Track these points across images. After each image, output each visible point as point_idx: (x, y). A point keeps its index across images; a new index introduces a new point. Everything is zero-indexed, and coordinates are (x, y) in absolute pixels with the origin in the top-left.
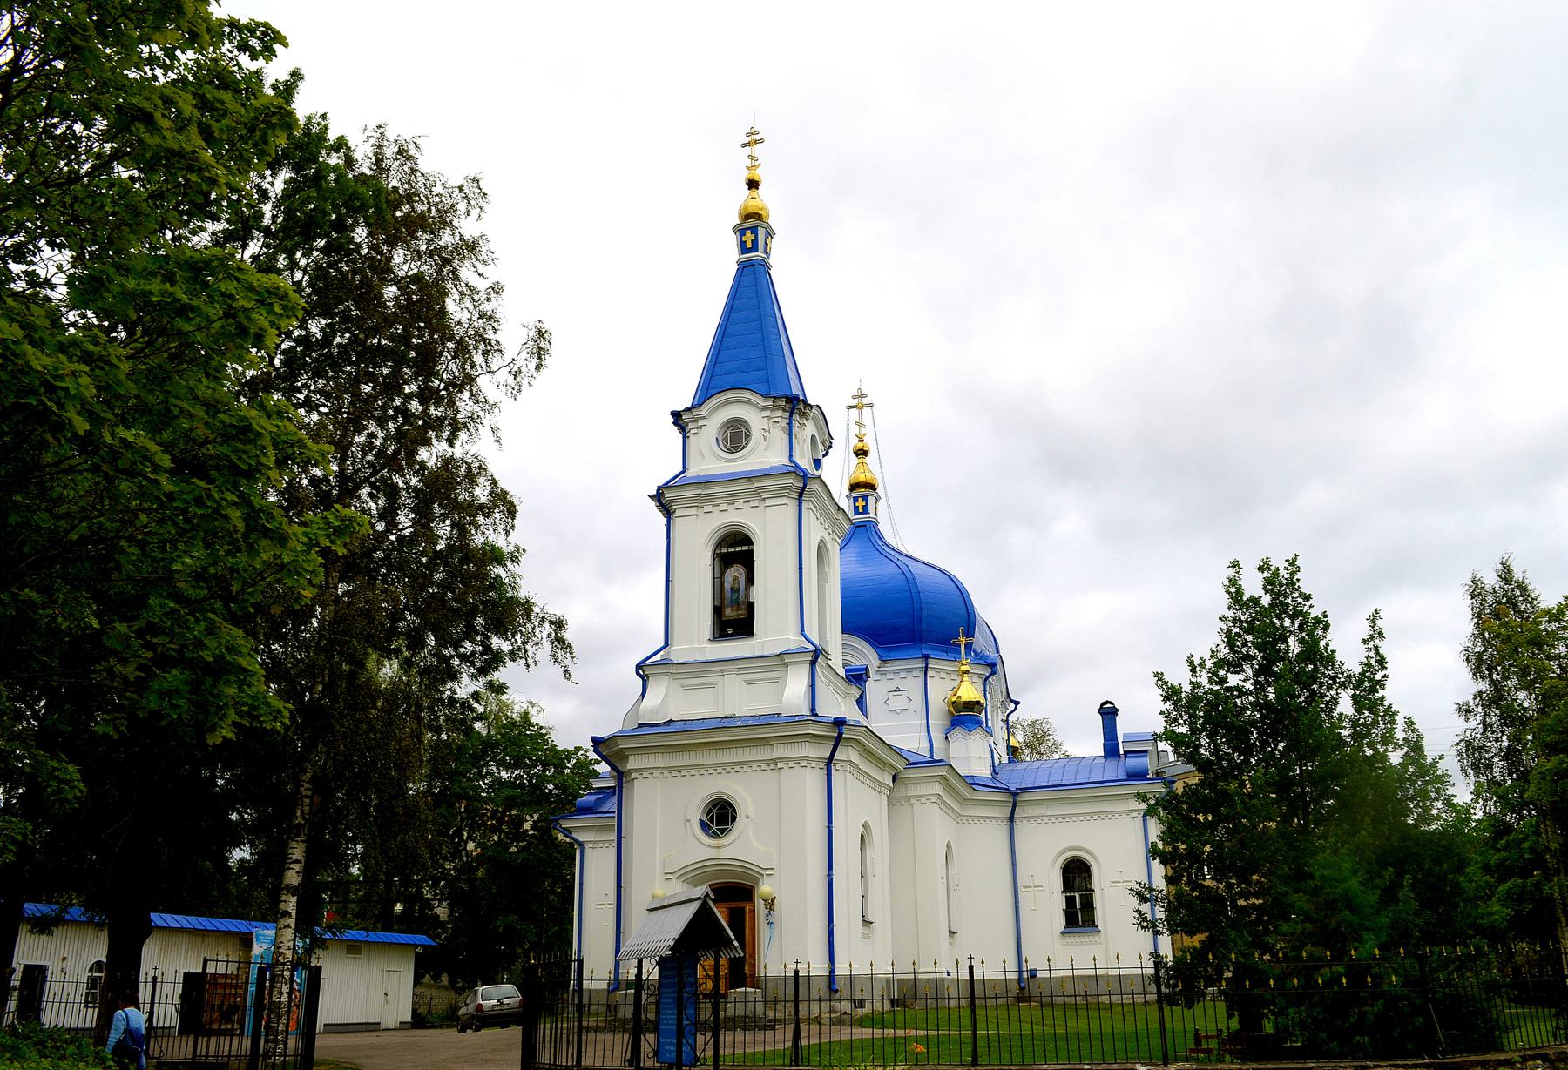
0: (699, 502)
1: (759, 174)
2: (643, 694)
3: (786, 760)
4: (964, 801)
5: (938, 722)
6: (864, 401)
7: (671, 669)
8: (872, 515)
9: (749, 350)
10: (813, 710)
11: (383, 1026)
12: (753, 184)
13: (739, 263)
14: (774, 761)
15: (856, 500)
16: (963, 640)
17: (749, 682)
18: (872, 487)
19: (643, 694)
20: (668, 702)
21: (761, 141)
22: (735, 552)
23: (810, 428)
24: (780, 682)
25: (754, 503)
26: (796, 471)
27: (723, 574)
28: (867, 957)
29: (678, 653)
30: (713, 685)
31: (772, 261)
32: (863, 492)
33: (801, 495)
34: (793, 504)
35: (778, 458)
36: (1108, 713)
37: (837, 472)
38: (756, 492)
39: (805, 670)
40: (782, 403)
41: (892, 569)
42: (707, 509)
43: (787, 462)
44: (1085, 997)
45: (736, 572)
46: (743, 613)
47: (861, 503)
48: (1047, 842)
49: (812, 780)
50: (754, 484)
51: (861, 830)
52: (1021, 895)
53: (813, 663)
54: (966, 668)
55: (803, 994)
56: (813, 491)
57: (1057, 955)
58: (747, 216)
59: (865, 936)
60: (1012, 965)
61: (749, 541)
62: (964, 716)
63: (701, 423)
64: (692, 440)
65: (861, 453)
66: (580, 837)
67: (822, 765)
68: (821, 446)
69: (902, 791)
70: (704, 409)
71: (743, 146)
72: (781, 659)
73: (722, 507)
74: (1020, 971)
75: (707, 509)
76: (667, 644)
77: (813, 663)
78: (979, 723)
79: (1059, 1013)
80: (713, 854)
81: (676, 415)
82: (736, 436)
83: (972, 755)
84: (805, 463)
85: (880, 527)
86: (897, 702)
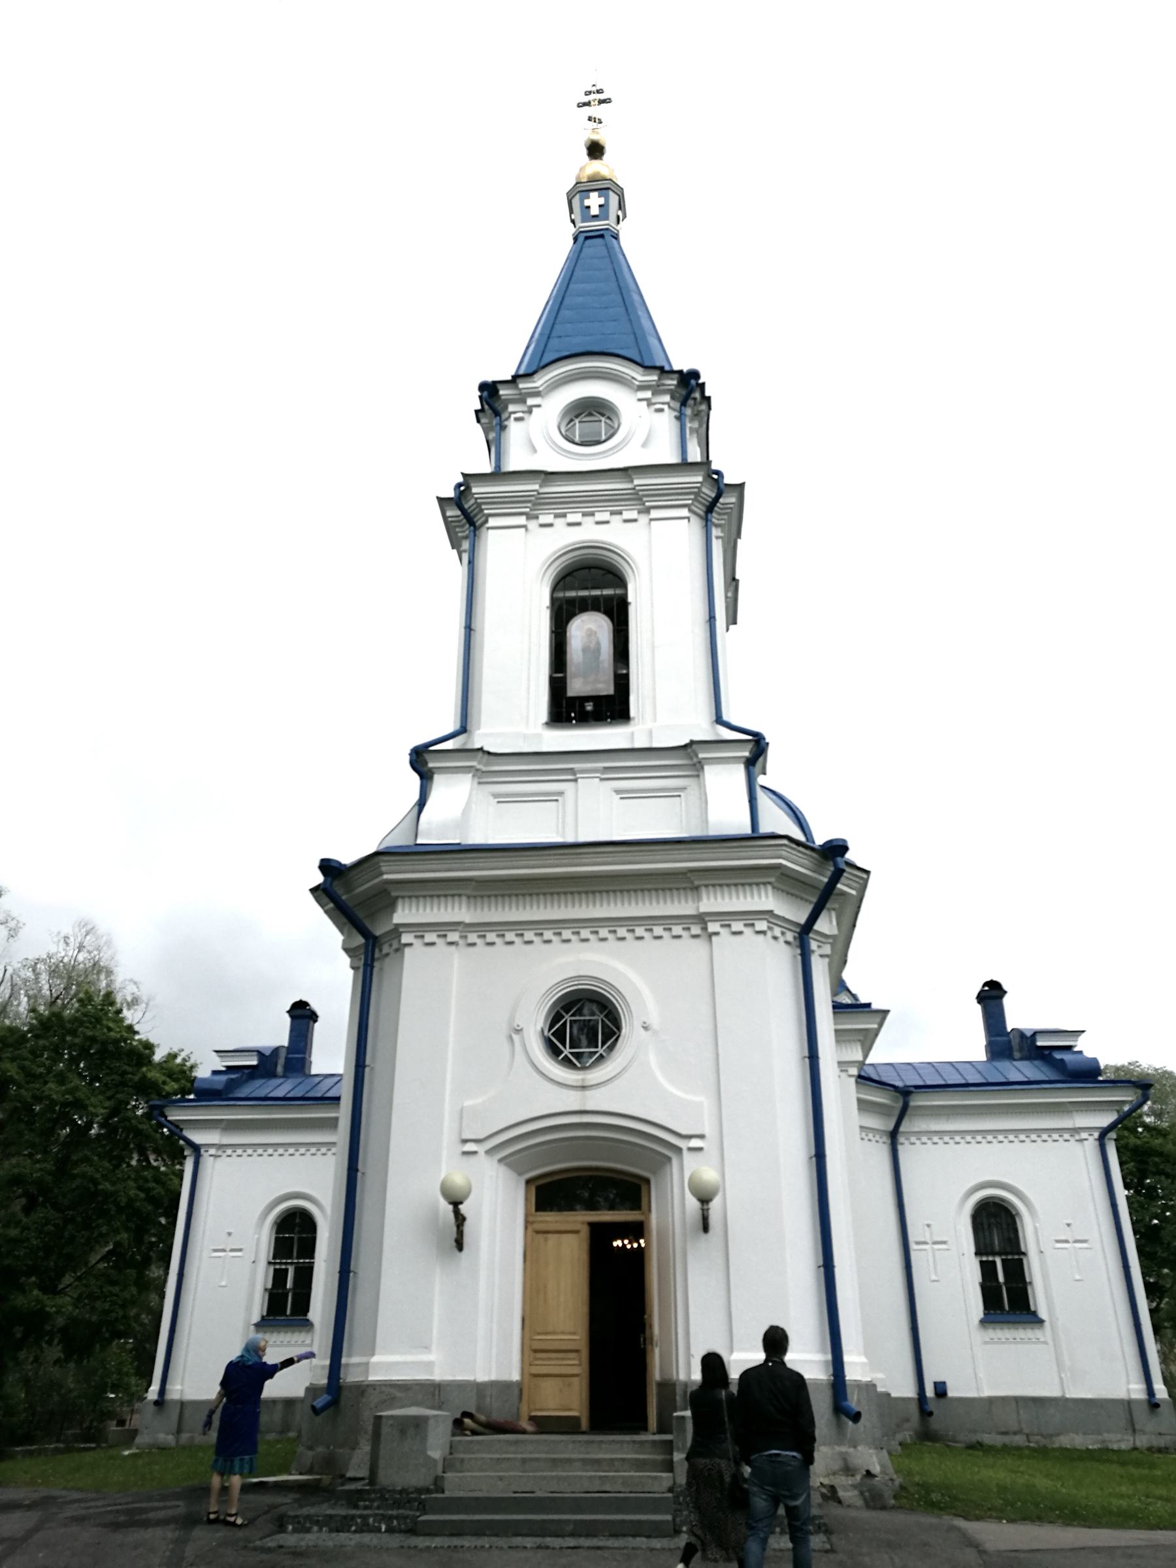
0: (534, 506)
2: (421, 804)
3: (726, 918)
11: (874, 1007)
12: (595, 150)
14: (702, 919)
19: (421, 804)
20: (462, 811)
22: (590, 587)
25: (627, 515)
33: (710, 508)
34: (696, 524)
42: (543, 519)
48: (952, 1170)
50: (634, 489)
52: (914, 1256)
57: (982, 1366)
61: (619, 580)
63: (531, 401)
66: (197, 1137)
70: (540, 381)
72: (690, 757)
80: (571, 1101)
81: (489, 391)
82: (591, 416)
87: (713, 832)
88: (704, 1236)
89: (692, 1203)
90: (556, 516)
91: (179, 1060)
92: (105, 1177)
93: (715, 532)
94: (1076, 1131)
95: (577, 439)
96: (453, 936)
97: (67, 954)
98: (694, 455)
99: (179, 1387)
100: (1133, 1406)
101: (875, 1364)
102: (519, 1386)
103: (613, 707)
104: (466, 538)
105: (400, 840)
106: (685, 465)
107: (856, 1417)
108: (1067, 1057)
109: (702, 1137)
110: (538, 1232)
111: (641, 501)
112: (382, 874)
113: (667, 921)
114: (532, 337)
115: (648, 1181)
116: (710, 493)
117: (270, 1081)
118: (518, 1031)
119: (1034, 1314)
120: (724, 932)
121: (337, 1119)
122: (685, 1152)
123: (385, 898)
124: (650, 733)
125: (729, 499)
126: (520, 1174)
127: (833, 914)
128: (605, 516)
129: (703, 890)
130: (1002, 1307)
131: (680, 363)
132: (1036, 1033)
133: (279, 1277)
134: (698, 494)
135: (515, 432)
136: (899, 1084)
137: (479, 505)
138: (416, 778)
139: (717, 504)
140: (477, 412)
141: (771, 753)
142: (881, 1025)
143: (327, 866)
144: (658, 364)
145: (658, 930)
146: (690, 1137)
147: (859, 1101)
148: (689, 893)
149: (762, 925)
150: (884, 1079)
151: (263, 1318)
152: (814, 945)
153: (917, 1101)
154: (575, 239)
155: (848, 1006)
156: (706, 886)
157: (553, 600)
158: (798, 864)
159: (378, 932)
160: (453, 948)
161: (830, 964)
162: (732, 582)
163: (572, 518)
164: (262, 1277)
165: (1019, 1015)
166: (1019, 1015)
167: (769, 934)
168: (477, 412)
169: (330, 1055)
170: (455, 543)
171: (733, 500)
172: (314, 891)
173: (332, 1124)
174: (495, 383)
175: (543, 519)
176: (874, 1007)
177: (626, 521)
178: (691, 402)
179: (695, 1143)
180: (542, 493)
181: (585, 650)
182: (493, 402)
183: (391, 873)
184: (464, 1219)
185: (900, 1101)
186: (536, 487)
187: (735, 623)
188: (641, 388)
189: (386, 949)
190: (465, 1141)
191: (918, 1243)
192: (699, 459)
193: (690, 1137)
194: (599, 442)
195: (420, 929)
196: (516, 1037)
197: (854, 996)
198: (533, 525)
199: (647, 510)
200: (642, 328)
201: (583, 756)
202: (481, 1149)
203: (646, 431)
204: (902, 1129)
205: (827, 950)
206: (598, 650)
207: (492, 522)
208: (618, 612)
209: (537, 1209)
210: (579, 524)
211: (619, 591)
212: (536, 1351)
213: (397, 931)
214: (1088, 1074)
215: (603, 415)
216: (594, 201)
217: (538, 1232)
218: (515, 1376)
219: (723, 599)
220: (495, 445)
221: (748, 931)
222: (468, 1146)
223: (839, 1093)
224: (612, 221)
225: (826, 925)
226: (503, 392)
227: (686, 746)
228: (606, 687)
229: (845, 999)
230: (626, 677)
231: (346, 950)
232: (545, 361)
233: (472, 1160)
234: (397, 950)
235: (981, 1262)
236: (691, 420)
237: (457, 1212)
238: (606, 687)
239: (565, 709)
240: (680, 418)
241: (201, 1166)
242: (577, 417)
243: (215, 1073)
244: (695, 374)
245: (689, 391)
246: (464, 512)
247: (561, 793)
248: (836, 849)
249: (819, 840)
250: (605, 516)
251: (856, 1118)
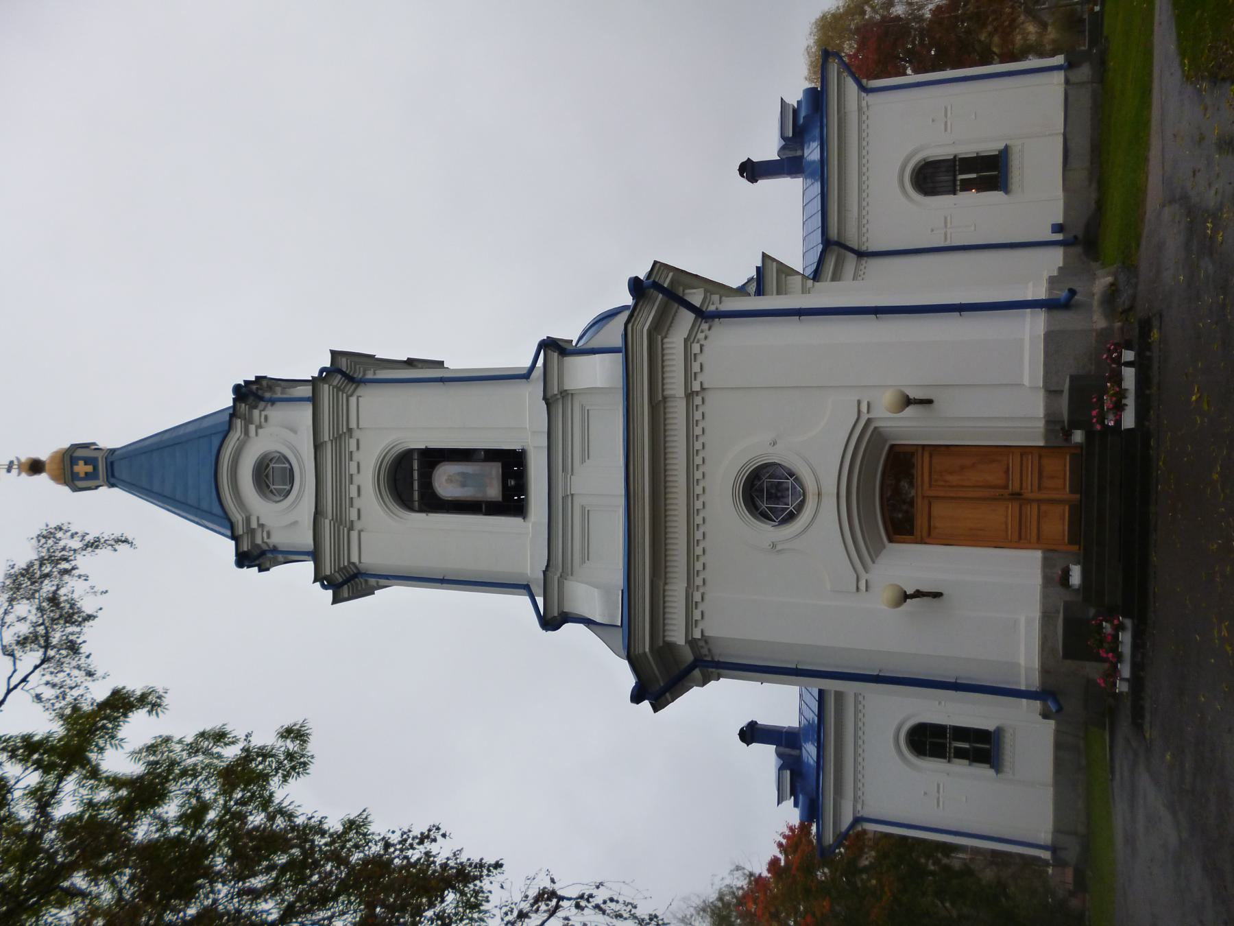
0: (344, 525)
2: (588, 622)
3: (689, 376)
11: (760, 264)
14: (690, 395)
20: (597, 587)
22: (413, 479)
25: (353, 447)
30: (586, 513)
33: (351, 379)
34: (364, 391)
36: (752, 171)
42: (354, 516)
48: (890, 210)
50: (332, 441)
57: (1040, 196)
61: (407, 455)
63: (254, 525)
66: (847, 820)
70: (238, 517)
80: (829, 503)
81: (243, 560)
82: (273, 476)
87: (619, 383)
88: (935, 404)
89: (910, 411)
90: (351, 505)
91: (784, 841)
93: (370, 375)
94: (860, 109)
95: (288, 487)
96: (697, 597)
98: (307, 391)
99: (1043, 835)
101: (1036, 274)
102: (1045, 551)
103: (512, 463)
104: (366, 582)
105: (619, 637)
106: (314, 400)
107: (1072, 292)
108: (803, 114)
109: (859, 402)
110: (929, 534)
111: (343, 434)
112: (645, 653)
113: (690, 423)
114: (197, 523)
115: (892, 446)
116: (338, 379)
117: (804, 763)
118: (774, 545)
119: (1000, 152)
120: (700, 378)
121: (836, 692)
122: (870, 416)
123: (665, 651)
124: (534, 433)
125: (343, 364)
126: (884, 547)
127: (687, 291)
128: (353, 466)
129: (666, 393)
130: (996, 176)
131: (227, 400)
132: (783, 137)
133: (960, 754)
135: (280, 538)
136: (820, 247)
137: (340, 569)
138: (568, 627)
139: (348, 371)
140: (260, 570)
141: (556, 335)
142: (774, 260)
143: (637, 697)
144: (228, 418)
145: (698, 431)
146: (859, 411)
147: (833, 279)
148: (668, 404)
149: (696, 348)
150: (816, 260)
151: (992, 767)
152: (712, 308)
153: (833, 234)
154: (112, 485)
155: (760, 283)
156: (663, 390)
157: (421, 511)
158: (647, 318)
159: (690, 657)
160: (706, 597)
161: (728, 296)
162: (411, 363)
163: (354, 493)
164: (961, 768)
165: (768, 149)
166: (768, 149)
167: (702, 342)
168: (260, 570)
169: (782, 705)
170: (369, 592)
171: (344, 360)
172: (656, 709)
173: (839, 696)
174: (237, 554)
175: (354, 516)
176: (760, 264)
177: (358, 448)
178: (260, 392)
179: (864, 408)
180: (333, 519)
181: (463, 485)
182: (254, 555)
184: (918, 591)
185: (835, 248)
186: (327, 522)
187: (442, 363)
188: (247, 433)
189: (705, 651)
190: (858, 589)
191: (946, 239)
192: (310, 388)
193: (859, 411)
194: (291, 470)
195: (690, 623)
196: (779, 547)
197: (750, 280)
198: (358, 525)
199: (350, 430)
200: (195, 432)
201: (553, 485)
202: (864, 577)
203: (286, 432)
204: (856, 247)
205: (716, 298)
206: (464, 475)
207: (355, 559)
208: (433, 457)
209: (912, 534)
210: (359, 488)
211: (416, 456)
212: (1020, 538)
213: (692, 642)
214: (816, 99)
215: (268, 465)
216: (81, 468)
217: (929, 534)
218: (1038, 555)
219: (421, 373)
220: (290, 556)
221: (700, 359)
222: (862, 587)
223: (827, 295)
224: (99, 454)
225: (696, 298)
226: (245, 547)
227: (548, 404)
228: (495, 469)
229: (753, 288)
230: (487, 451)
231: (704, 683)
232: (220, 512)
234: (706, 642)
235: (962, 190)
236: (274, 392)
237: (912, 596)
238: (495, 469)
239: (512, 503)
240: (273, 402)
241: (872, 817)
242: (268, 487)
243: (796, 805)
244: (237, 389)
245: (253, 394)
246: (345, 582)
247: (583, 508)
248: (636, 286)
249: (628, 300)
250: (353, 466)
251: (846, 283)
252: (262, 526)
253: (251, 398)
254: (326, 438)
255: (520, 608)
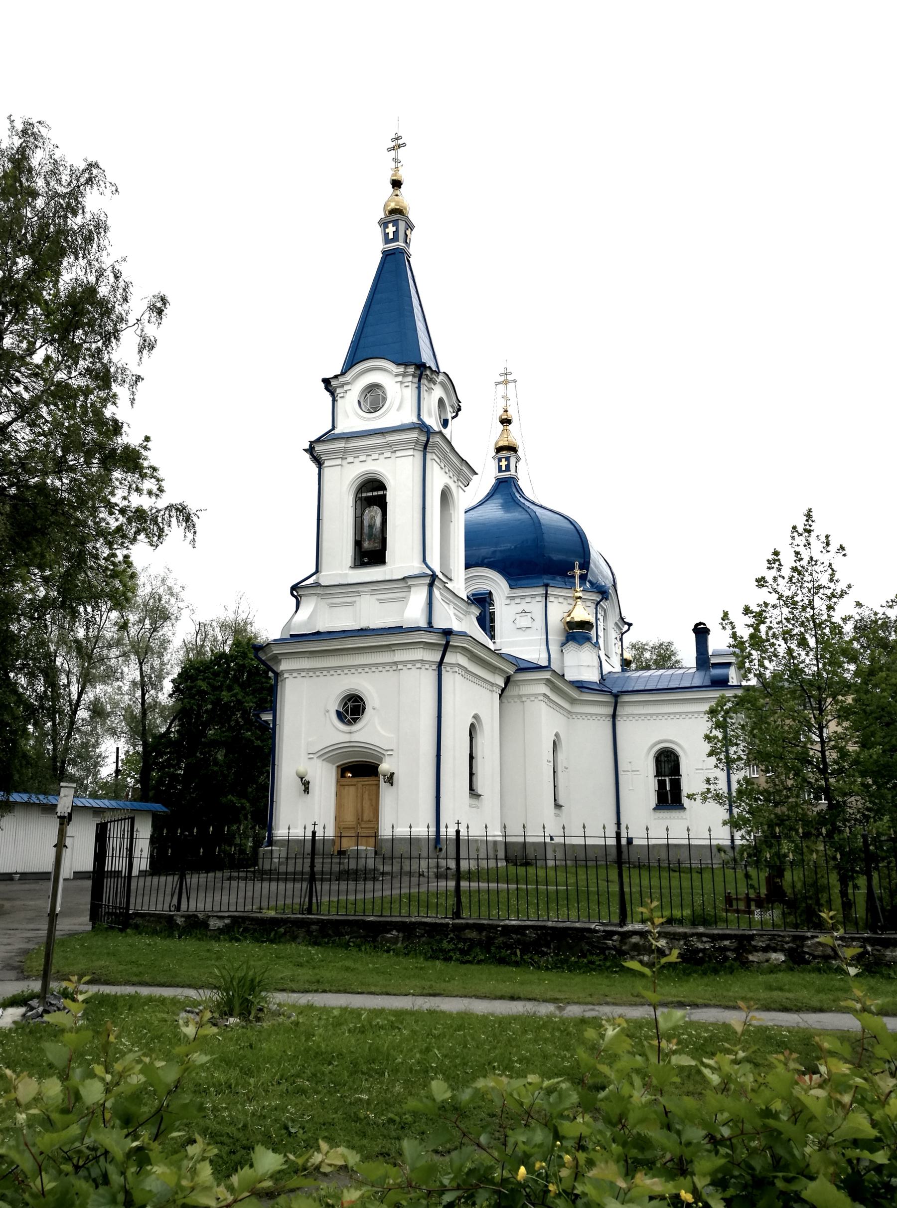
1: (403, 175)
4: (573, 701)
5: (555, 639)
6: (510, 378)
7: (318, 591)
8: (513, 472)
9: (389, 324)
10: (430, 623)
12: (396, 184)
13: (383, 252)
14: (395, 663)
15: (500, 460)
16: (578, 572)
17: (381, 601)
18: (513, 449)
20: (315, 616)
21: (404, 145)
22: (372, 494)
23: (438, 392)
24: (404, 600)
26: (422, 428)
27: (362, 514)
28: (477, 821)
29: (325, 578)
30: (352, 604)
31: (412, 250)
32: (504, 454)
34: (419, 455)
35: (410, 418)
37: (472, 436)
38: (389, 445)
39: (424, 591)
40: (411, 370)
41: (525, 516)
43: (415, 420)
44: (672, 862)
45: (375, 512)
46: (377, 546)
47: (504, 463)
49: (428, 678)
51: (553, 738)
53: (431, 585)
54: (580, 594)
55: (463, 854)
56: (436, 445)
57: (648, 826)
58: (393, 212)
59: (556, 815)
60: (611, 831)
61: (382, 486)
62: (577, 633)
63: (346, 388)
64: (340, 403)
65: (506, 422)
67: (434, 667)
68: (449, 409)
69: (512, 691)
71: (389, 150)
73: (362, 458)
74: (618, 836)
75: (350, 459)
76: (317, 571)
77: (431, 585)
78: (589, 639)
79: (655, 874)
80: (347, 738)
81: (326, 382)
82: (374, 397)
83: (581, 664)
84: (433, 422)
85: (521, 483)
86: (524, 622)
92: (257, 739)
97: (230, 617)
100: (527, 846)
111: (391, 447)
113: (384, 665)
116: (423, 438)
134: (417, 442)
179: (389, 753)
183: (276, 650)
186: (343, 445)
188: (396, 376)
195: (291, 671)
198: (345, 462)
202: (315, 756)
211: (381, 493)
232: (355, 362)
233: (312, 761)
235: (659, 781)
247: (355, 602)
252: (346, 391)
253: (418, 372)
254: (388, 439)
255: (304, 568)
